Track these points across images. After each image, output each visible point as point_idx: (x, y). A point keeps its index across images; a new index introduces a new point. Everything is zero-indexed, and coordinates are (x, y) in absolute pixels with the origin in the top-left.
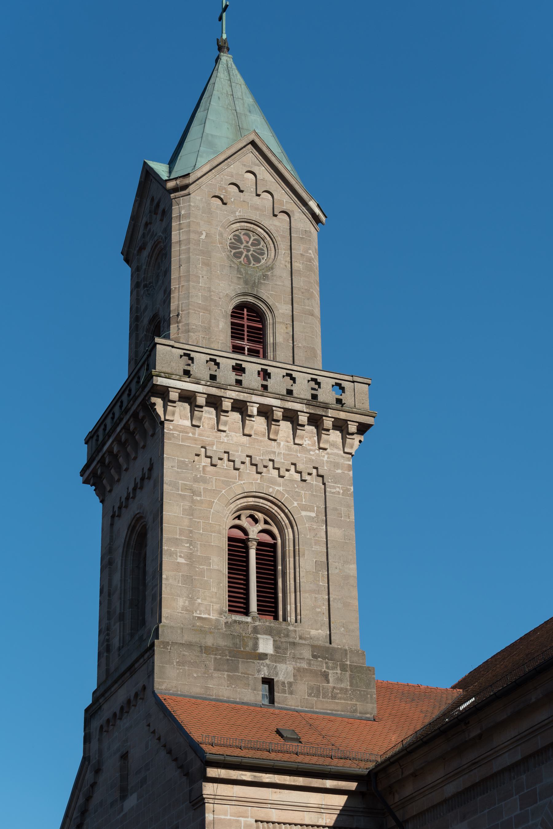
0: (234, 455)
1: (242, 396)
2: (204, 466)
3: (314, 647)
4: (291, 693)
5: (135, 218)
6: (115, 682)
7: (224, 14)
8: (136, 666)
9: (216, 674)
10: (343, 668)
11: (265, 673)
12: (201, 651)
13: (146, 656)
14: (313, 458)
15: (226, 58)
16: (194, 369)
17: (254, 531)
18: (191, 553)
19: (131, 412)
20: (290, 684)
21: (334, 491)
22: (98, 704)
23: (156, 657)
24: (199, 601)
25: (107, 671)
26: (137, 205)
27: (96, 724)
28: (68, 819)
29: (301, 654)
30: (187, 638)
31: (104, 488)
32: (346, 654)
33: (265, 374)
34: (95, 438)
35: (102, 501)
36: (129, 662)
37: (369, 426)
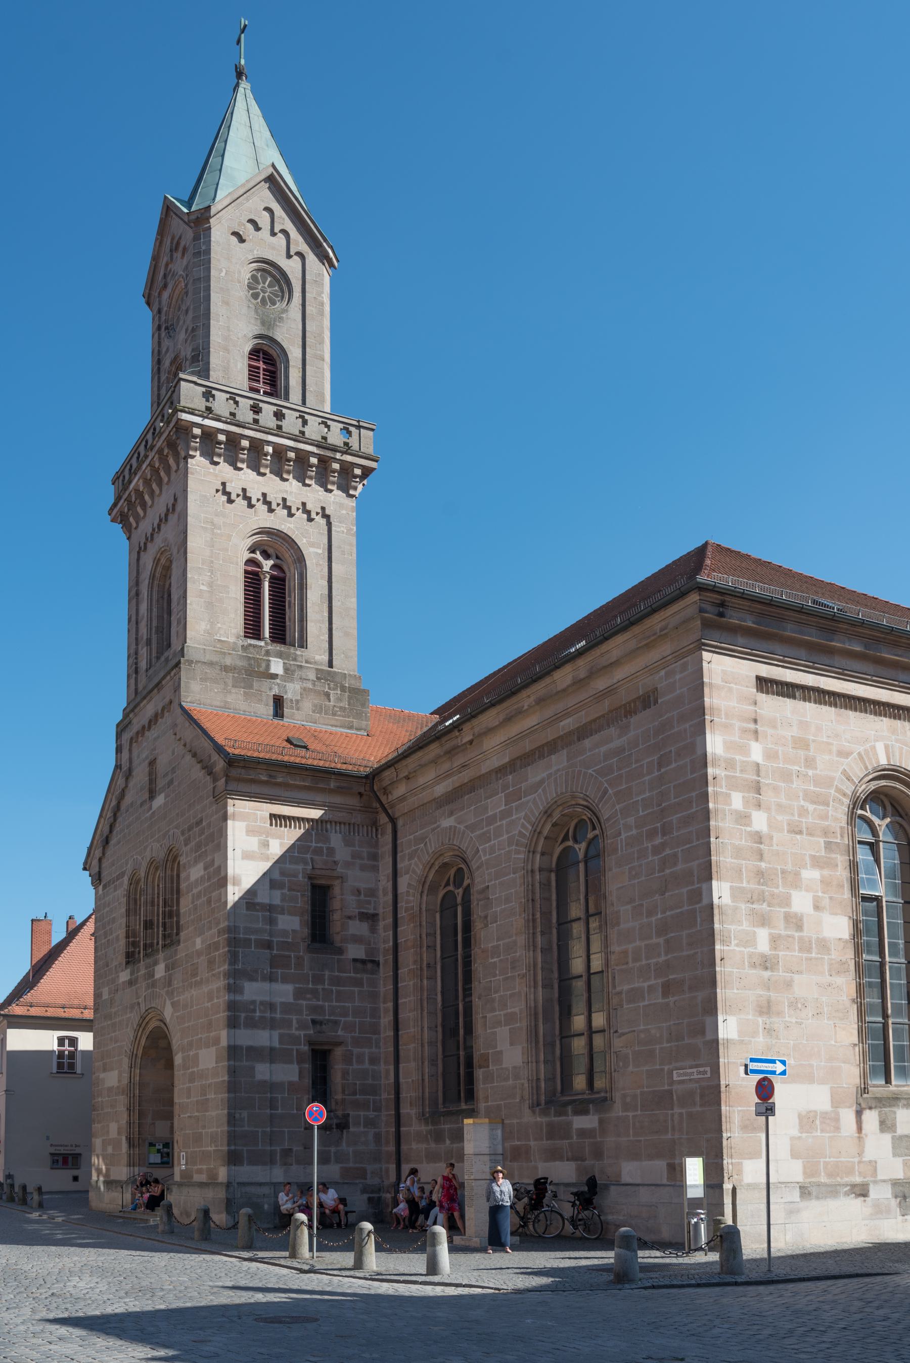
0: (250, 492)
3: (318, 671)
4: (298, 709)
5: (156, 258)
6: (144, 698)
7: (243, 35)
8: (163, 682)
9: (234, 690)
10: (343, 689)
11: (276, 691)
12: (221, 670)
13: (172, 674)
14: (322, 498)
15: (244, 85)
18: (212, 582)
19: (156, 449)
20: (297, 701)
21: (339, 530)
22: (128, 719)
23: (183, 673)
24: (219, 625)
26: (158, 244)
27: (126, 736)
28: (102, 820)
29: (307, 676)
30: (208, 657)
31: (131, 525)
32: (345, 677)
33: (279, 415)
34: (121, 478)
35: (128, 539)
36: (156, 680)
37: (373, 469)
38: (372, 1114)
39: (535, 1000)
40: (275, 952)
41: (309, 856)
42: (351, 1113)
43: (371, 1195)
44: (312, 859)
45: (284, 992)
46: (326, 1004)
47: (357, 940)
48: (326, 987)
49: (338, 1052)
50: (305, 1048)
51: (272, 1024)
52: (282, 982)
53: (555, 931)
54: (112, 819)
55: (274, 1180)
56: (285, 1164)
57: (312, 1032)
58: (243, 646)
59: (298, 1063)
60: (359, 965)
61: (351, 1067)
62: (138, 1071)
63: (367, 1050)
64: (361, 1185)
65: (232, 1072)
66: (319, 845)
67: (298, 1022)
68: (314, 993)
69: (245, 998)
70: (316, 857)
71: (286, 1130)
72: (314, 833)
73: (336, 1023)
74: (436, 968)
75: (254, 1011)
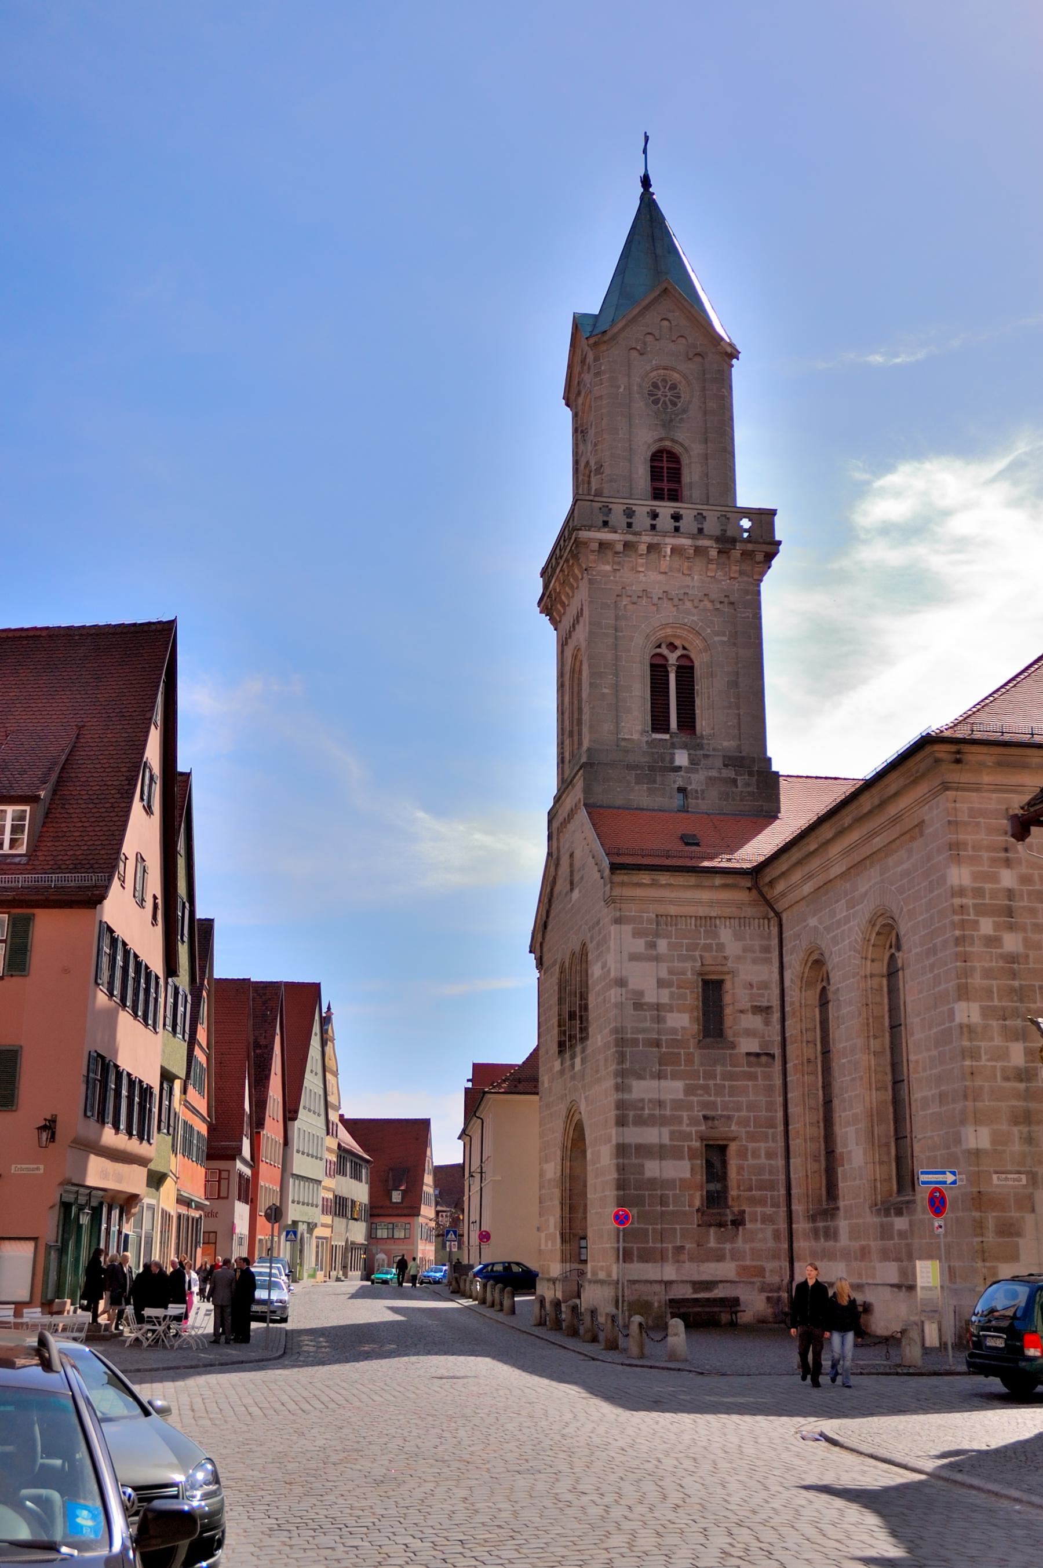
1: (656, 540)
2: (625, 605)
4: (703, 799)
8: (575, 780)
11: (680, 783)
16: (613, 519)
17: (673, 658)
20: (703, 791)
21: (743, 615)
25: (563, 779)
32: (754, 762)
33: (676, 517)
38: (769, 1210)
39: (871, 1103)
40: (664, 1050)
41: (697, 953)
42: (747, 1210)
43: (770, 1295)
44: (701, 957)
45: (673, 1089)
46: (719, 1099)
47: (749, 1033)
48: (718, 1082)
49: (733, 1148)
50: (696, 1144)
51: (663, 1121)
52: (672, 1079)
53: (887, 1035)
54: (547, 906)
55: (666, 1278)
56: (678, 1262)
57: (703, 1128)
58: (647, 742)
59: (690, 1159)
60: (753, 1059)
61: (746, 1162)
62: (568, 1164)
63: (763, 1145)
64: (758, 1284)
65: (621, 1169)
66: (707, 942)
67: (689, 1119)
68: (706, 1089)
69: (633, 1097)
70: (705, 954)
71: (678, 1227)
72: (702, 930)
73: (729, 1118)
74: (816, 1063)
75: (643, 1109)
